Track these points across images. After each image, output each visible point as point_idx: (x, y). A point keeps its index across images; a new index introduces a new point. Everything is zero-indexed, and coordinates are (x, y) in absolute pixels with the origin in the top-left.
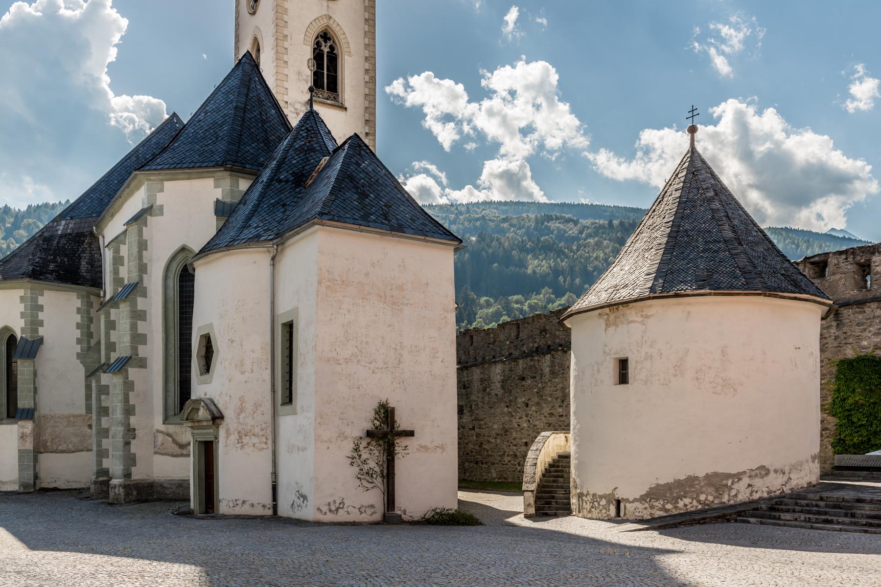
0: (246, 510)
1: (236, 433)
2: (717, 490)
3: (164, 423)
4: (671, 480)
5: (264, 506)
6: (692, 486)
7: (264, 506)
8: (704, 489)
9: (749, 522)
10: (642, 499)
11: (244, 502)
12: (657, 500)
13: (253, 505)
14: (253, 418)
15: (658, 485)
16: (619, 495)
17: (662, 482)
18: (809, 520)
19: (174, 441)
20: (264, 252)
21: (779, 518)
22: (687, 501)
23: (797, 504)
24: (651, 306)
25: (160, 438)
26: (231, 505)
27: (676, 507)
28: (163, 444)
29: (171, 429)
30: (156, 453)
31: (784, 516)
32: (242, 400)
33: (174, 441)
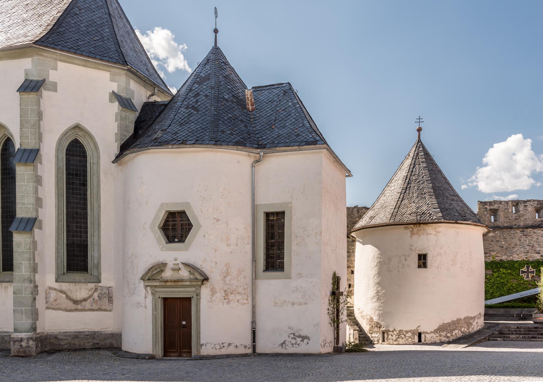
0: (231, 350)
1: (222, 292)
2: (468, 326)
3: (56, 281)
4: (450, 321)
5: (245, 347)
6: (459, 324)
7: (245, 347)
8: (463, 325)
9: (497, 340)
10: (435, 331)
11: (229, 344)
12: (443, 332)
13: (237, 347)
14: (238, 281)
15: (444, 324)
16: (421, 330)
17: (446, 322)
18: (525, 338)
19: (68, 297)
20: (246, 155)
21: (509, 337)
22: (457, 331)
23: (509, 330)
24: (440, 227)
25: (53, 294)
26: (218, 347)
27: (452, 335)
28: (55, 300)
29: (65, 286)
30: (47, 308)
31: (511, 336)
32: (228, 266)
33: (68, 297)
